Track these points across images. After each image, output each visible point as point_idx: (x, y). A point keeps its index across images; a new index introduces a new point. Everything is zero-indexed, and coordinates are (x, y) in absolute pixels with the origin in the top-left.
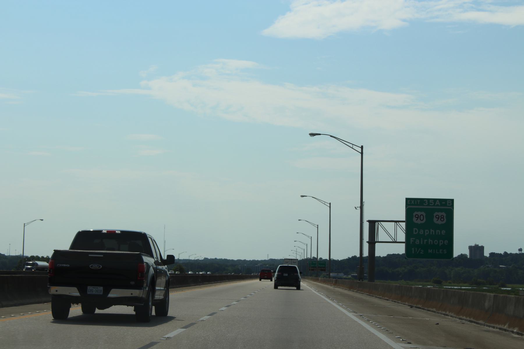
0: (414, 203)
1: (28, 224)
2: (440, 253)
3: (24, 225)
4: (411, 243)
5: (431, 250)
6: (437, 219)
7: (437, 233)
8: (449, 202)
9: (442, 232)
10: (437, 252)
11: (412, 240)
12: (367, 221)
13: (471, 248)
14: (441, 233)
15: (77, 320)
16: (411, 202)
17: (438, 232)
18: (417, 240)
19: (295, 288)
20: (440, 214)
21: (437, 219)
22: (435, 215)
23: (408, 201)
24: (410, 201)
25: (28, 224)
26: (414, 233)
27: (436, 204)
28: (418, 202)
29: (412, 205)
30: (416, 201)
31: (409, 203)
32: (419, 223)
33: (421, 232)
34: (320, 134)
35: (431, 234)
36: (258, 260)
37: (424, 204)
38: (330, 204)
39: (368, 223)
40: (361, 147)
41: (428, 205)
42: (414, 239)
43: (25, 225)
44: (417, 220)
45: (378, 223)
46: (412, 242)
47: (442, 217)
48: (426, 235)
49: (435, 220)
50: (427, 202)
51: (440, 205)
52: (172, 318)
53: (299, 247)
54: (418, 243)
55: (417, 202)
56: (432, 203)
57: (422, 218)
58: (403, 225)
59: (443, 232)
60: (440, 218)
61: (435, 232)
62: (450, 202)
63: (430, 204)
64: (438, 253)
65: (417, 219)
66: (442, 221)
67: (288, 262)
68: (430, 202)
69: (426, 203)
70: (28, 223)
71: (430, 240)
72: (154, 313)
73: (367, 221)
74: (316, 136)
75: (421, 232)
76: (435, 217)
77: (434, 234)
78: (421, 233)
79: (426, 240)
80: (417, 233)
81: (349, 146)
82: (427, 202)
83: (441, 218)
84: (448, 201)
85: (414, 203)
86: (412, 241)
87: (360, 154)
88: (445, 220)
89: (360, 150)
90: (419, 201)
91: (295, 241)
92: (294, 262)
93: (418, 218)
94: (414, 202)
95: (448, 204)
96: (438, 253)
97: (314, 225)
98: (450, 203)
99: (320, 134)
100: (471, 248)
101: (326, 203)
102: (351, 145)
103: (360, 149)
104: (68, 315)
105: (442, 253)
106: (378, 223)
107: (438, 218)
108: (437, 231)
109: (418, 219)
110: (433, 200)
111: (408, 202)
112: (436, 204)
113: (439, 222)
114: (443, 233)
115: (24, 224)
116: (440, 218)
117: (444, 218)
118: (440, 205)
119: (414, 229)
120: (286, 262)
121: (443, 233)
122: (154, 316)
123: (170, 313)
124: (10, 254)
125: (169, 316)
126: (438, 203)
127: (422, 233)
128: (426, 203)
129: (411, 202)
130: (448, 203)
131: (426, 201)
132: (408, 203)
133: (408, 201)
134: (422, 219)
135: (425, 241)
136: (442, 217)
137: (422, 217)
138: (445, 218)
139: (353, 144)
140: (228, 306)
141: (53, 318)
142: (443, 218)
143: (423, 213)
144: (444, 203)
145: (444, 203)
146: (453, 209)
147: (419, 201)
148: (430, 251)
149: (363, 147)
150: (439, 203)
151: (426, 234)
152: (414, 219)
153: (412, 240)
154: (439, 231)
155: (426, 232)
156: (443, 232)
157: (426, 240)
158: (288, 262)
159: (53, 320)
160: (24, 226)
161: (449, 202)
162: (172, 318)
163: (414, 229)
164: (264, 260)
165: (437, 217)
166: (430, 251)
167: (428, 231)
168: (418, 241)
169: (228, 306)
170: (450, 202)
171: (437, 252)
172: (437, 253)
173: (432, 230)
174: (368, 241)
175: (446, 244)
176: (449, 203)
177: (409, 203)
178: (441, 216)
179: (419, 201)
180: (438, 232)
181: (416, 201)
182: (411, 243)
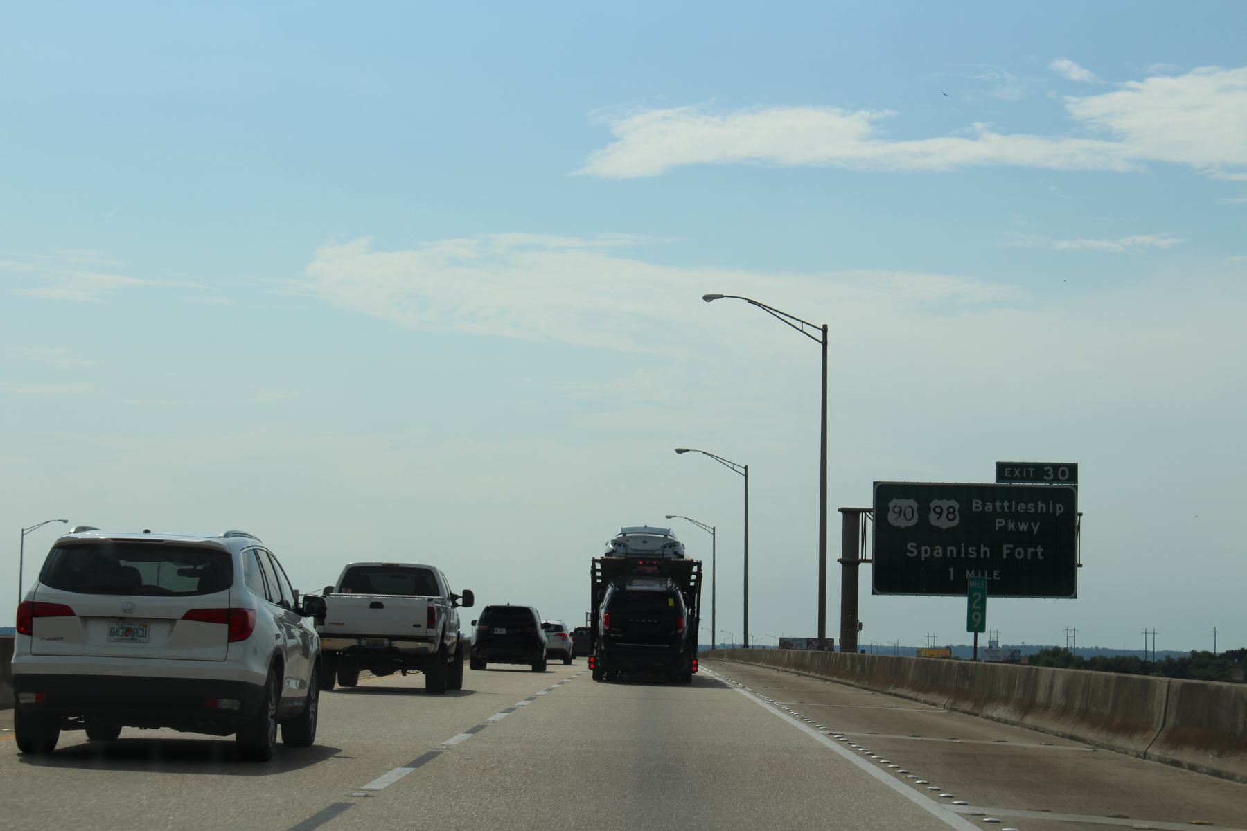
0: (1019, 476)
3: (21, 532)
4: (1005, 556)
7: (949, 555)
11: (1008, 549)
12: (839, 510)
14: (1016, 508)
15: (76, 757)
16: (1012, 472)
17: (952, 551)
19: (561, 662)
20: (945, 504)
23: (1006, 469)
24: (1010, 469)
25: (32, 529)
29: (1017, 479)
30: (1025, 470)
31: (1010, 476)
33: (937, 551)
34: (722, 297)
37: (1045, 478)
38: (825, 330)
39: (841, 515)
40: (821, 327)
41: (1056, 479)
42: (1012, 546)
43: (25, 532)
44: (938, 519)
45: (866, 515)
46: (1007, 554)
48: (923, 559)
50: (1050, 473)
52: (325, 753)
55: (1028, 472)
65: (938, 516)
69: (1050, 475)
72: (279, 739)
73: (839, 510)
74: (714, 300)
75: (937, 551)
77: (1044, 511)
78: (938, 553)
79: (1033, 550)
81: (789, 322)
82: (1050, 473)
83: (949, 513)
85: (1019, 476)
88: (958, 517)
94: (1021, 473)
96: (990, 578)
97: (705, 527)
99: (722, 297)
101: (806, 328)
103: (821, 333)
104: (119, 734)
106: (866, 515)
107: (941, 514)
108: (949, 549)
109: (899, 516)
114: (1022, 509)
115: (23, 530)
116: (945, 512)
121: (1022, 509)
122: (279, 744)
123: (319, 740)
124: (157, 584)
125: (319, 744)
129: (1012, 472)
131: (1049, 470)
134: (909, 516)
135: (1030, 550)
137: (909, 510)
138: (956, 513)
139: (803, 322)
140: (509, 711)
141: (88, 738)
142: (953, 513)
143: (954, 503)
146: (1075, 491)
151: (924, 556)
153: (1008, 549)
155: (923, 552)
157: (1033, 550)
159: (88, 740)
160: (23, 535)
162: (325, 753)
165: (938, 510)
169: (509, 711)
174: (841, 557)
177: (1008, 474)
178: (948, 509)
180: (952, 551)
181: (1025, 470)
182: (1005, 556)
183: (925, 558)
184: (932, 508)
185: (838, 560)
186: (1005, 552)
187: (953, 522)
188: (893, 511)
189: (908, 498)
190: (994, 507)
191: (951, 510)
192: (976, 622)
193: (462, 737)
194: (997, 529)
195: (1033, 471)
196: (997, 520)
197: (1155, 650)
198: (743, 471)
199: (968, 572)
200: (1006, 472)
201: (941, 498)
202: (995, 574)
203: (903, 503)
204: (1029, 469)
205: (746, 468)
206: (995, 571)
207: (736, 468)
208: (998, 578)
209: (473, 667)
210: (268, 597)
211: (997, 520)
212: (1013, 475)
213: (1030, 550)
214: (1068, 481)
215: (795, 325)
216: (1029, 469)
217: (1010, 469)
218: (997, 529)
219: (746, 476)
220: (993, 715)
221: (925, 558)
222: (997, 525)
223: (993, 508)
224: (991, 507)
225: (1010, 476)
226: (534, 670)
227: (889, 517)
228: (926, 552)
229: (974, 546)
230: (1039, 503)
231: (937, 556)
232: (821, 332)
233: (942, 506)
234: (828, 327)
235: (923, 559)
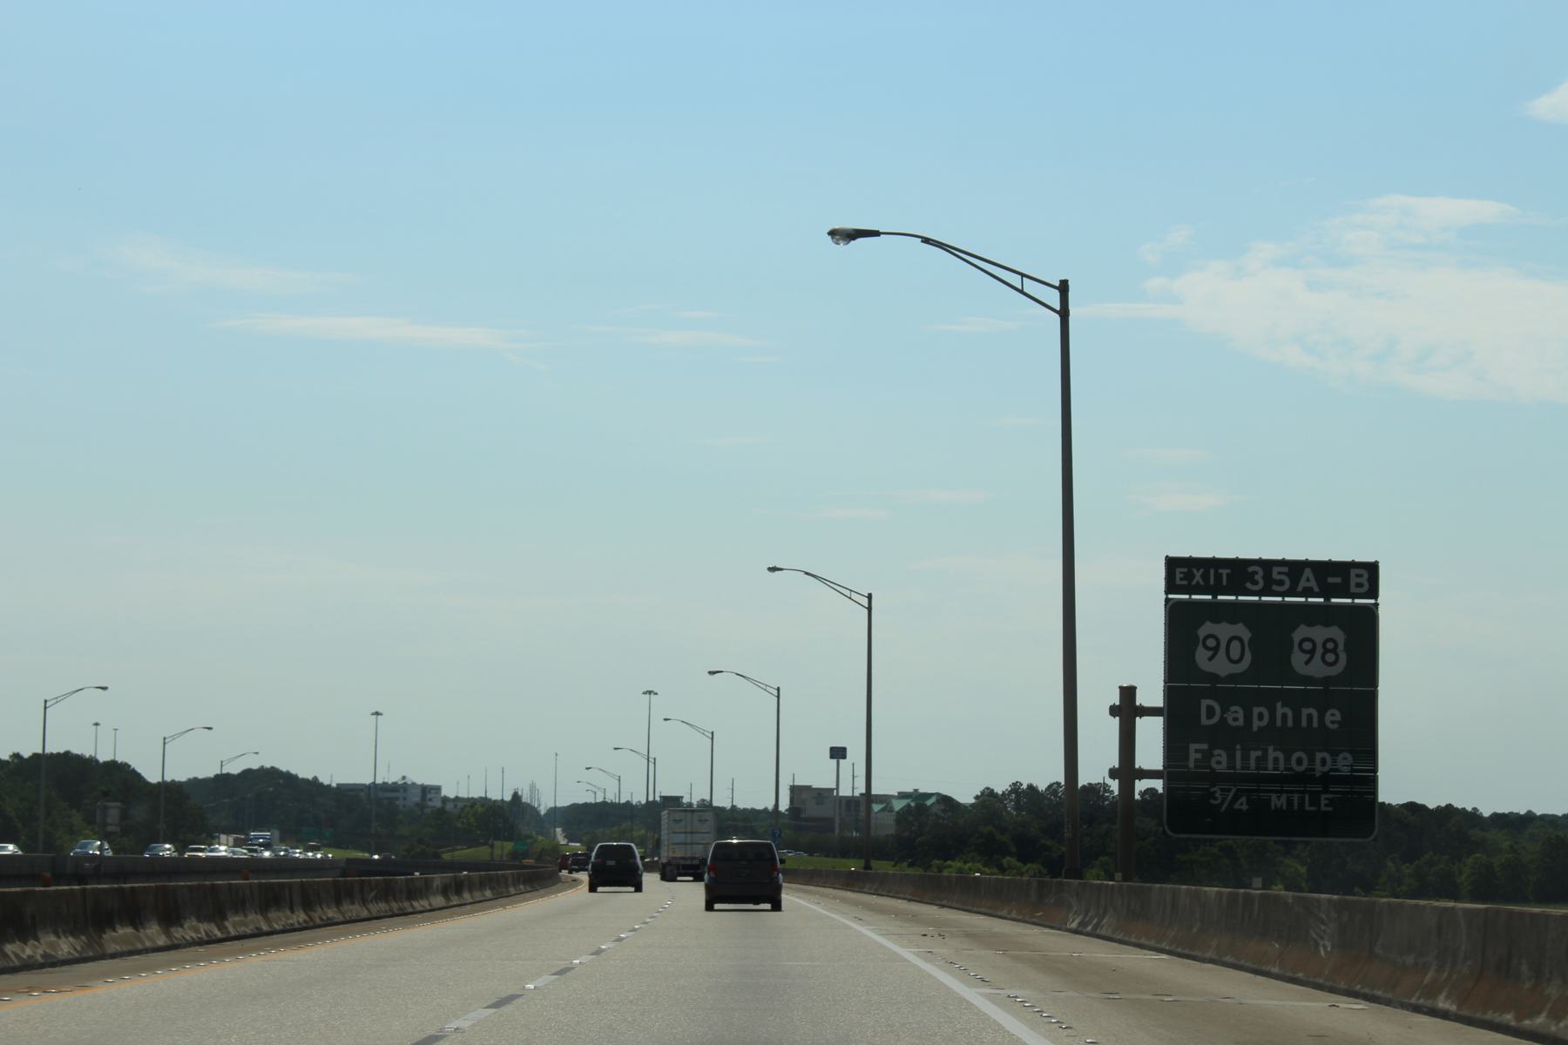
0: (1202, 582)
1: (57, 702)
2: (1323, 808)
6: (1308, 656)
7: (1304, 723)
9: (1328, 718)
10: (1310, 805)
13: (1061, 281)
16: (1189, 576)
17: (1310, 717)
18: (1216, 752)
19: (632, 889)
20: (1319, 633)
21: (1308, 656)
22: (1203, 631)
24: (1185, 570)
25: (57, 700)
26: (1204, 721)
27: (1300, 589)
30: (1212, 571)
31: (1185, 583)
34: (876, 234)
35: (1279, 723)
36: (67, 753)
37: (1249, 585)
40: (1057, 284)
42: (1205, 746)
43: (48, 704)
44: (1210, 659)
46: (1196, 760)
47: (1330, 645)
49: (1298, 660)
50: (1259, 577)
51: (1316, 589)
53: (389, 767)
55: (1218, 577)
56: (1281, 583)
59: (1333, 717)
60: (1320, 650)
63: (1275, 588)
64: (1313, 809)
65: (1210, 653)
67: (681, 821)
68: (1275, 576)
69: (1256, 583)
70: (56, 698)
71: (1272, 753)
77: (1290, 723)
79: (1259, 753)
80: (1216, 719)
82: (1259, 577)
83: (1326, 651)
84: (1353, 572)
85: (1202, 582)
86: (1193, 756)
87: (866, 611)
88: (1343, 657)
89: (1054, 299)
90: (1224, 572)
91: (616, 749)
92: (700, 821)
94: (1205, 577)
96: (1313, 809)
98: (1364, 580)
99: (876, 234)
100: (1061, 281)
102: (1015, 280)
107: (1312, 652)
108: (1305, 712)
110: (1285, 569)
111: (1178, 576)
112: (1300, 589)
113: (1317, 669)
114: (1333, 722)
116: (1320, 650)
118: (1316, 589)
119: (1205, 703)
120: (675, 820)
126: (1308, 580)
127: (1241, 722)
128: (1256, 583)
129: (1189, 576)
130: (1353, 580)
132: (1178, 582)
135: (1254, 754)
136: (1329, 647)
137: (1235, 645)
138: (1341, 647)
139: (1023, 275)
142: (1334, 651)
144: (1338, 580)
145: (1338, 580)
147: (1228, 571)
148: (1278, 802)
150: (1313, 584)
151: (1256, 724)
152: (1201, 656)
154: (1315, 713)
156: (1333, 715)
157: (1259, 753)
158: (681, 821)
160: (45, 708)
163: (1205, 703)
164: (247, 774)
165: (1307, 646)
167: (1266, 713)
168: (1219, 755)
171: (1310, 805)
172: (1307, 808)
173: (1283, 706)
175: (1328, 724)
176: (1359, 580)
178: (1324, 645)
179: (1228, 571)
180: (1310, 717)
181: (1212, 571)
183: (1259, 728)
184: (1201, 639)
186: (1193, 756)
187: (1334, 667)
191: (1330, 645)
193: (586, 958)
195: (1227, 574)
198: (865, 602)
201: (1311, 624)
202: (1323, 802)
204: (1221, 571)
205: (870, 597)
206: (1193, 747)
207: (1029, 286)
208: (1330, 809)
212: (1190, 583)
213: (1254, 754)
215: (1008, 281)
216: (1221, 571)
217: (1185, 570)
219: (870, 609)
221: (1259, 728)
225: (1185, 583)
226: (636, 891)
228: (1261, 717)
230: (1279, 705)
231: (1235, 724)
232: (1057, 294)
234: (1069, 283)
235: (1255, 728)
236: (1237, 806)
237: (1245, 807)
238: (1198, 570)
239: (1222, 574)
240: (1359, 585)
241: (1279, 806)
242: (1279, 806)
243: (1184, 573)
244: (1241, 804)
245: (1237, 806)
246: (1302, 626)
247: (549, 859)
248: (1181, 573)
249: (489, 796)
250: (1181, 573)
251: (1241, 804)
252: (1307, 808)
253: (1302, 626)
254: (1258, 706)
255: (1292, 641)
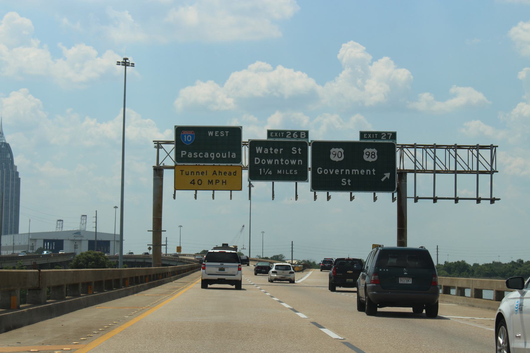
0: (371, 137)
2: (290, 173)
5: (281, 171)
7: (353, 173)
8: (302, 134)
9: (361, 172)
10: (287, 173)
16: (367, 136)
20: (371, 150)
22: (365, 151)
23: (365, 134)
26: (256, 163)
28: (282, 134)
29: (370, 139)
30: (373, 134)
32: (370, 161)
44: (368, 158)
47: (373, 153)
49: (365, 157)
54: (208, 157)
55: (375, 136)
57: (340, 156)
58: (171, 147)
60: (371, 155)
61: (351, 172)
62: (303, 134)
64: (288, 173)
65: (368, 156)
66: (373, 158)
76: (331, 153)
79: (343, 170)
83: (372, 155)
84: (301, 133)
93: (335, 155)
94: (278, 134)
95: (354, 170)
96: (288, 173)
98: (304, 135)
105: (292, 173)
107: (369, 155)
109: (368, 157)
113: (370, 160)
116: (371, 155)
117: (375, 155)
119: (256, 158)
121: (362, 173)
129: (274, 134)
130: (301, 135)
133: (365, 134)
134: (340, 156)
135: (342, 170)
137: (340, 154)
142: (374, 155)
148: (279, 172)
149: (195, 199)
157: (343, 170)
161: (302, 134)
163: (256, 158)
165: (368, 153)
166: (279, 172)
170: (303, 134)
171: (287, 173)
172: (287, 173)
176: (303, 135)
180: (224, 155)
181: (279, 133)
185: (153, 167)
187: (374, 159)
188: (332, 153)
189: (339, 148)
190: (269, 151)
192: (222, 269)
194: (182, 156)
195: (377, 135)
196: (182, 152)
197: (97, 231)
199: (278, 171)
200: (365, 136)
202: (291, 172)
203: (337, 150)
204: (282, 133)
206: (290, 170)
209: (62, 249)
210: (220, 173)
211: (182, 152)
213: (342, 170)
214: (391, 139)
216: (282, 133)
217: (273, 133)
218: (182, 156)
220: (512, 297)
222: (182, 154)
223: (268, 151)
224: (267, 151)
227: (364, 157)
229: (322, 168)
233: (370, 152)
236: (269, 173)
237: (271, 173)
238: (276, 133)
239: (226, 133)
240: (303, 136)
241: (279, 173)
242: (279, 173)
243: (218, 133)
244: (270, 173)
245: (269, 173)
246: (333, 148)
247: (248, 280)
248: (217, 133)
249: (100, 230)
250: (217, 133)
251: (270, 173)
252: (287, 173)
253: (333, 148)
254: (353, 169)
255: (330, 152)
